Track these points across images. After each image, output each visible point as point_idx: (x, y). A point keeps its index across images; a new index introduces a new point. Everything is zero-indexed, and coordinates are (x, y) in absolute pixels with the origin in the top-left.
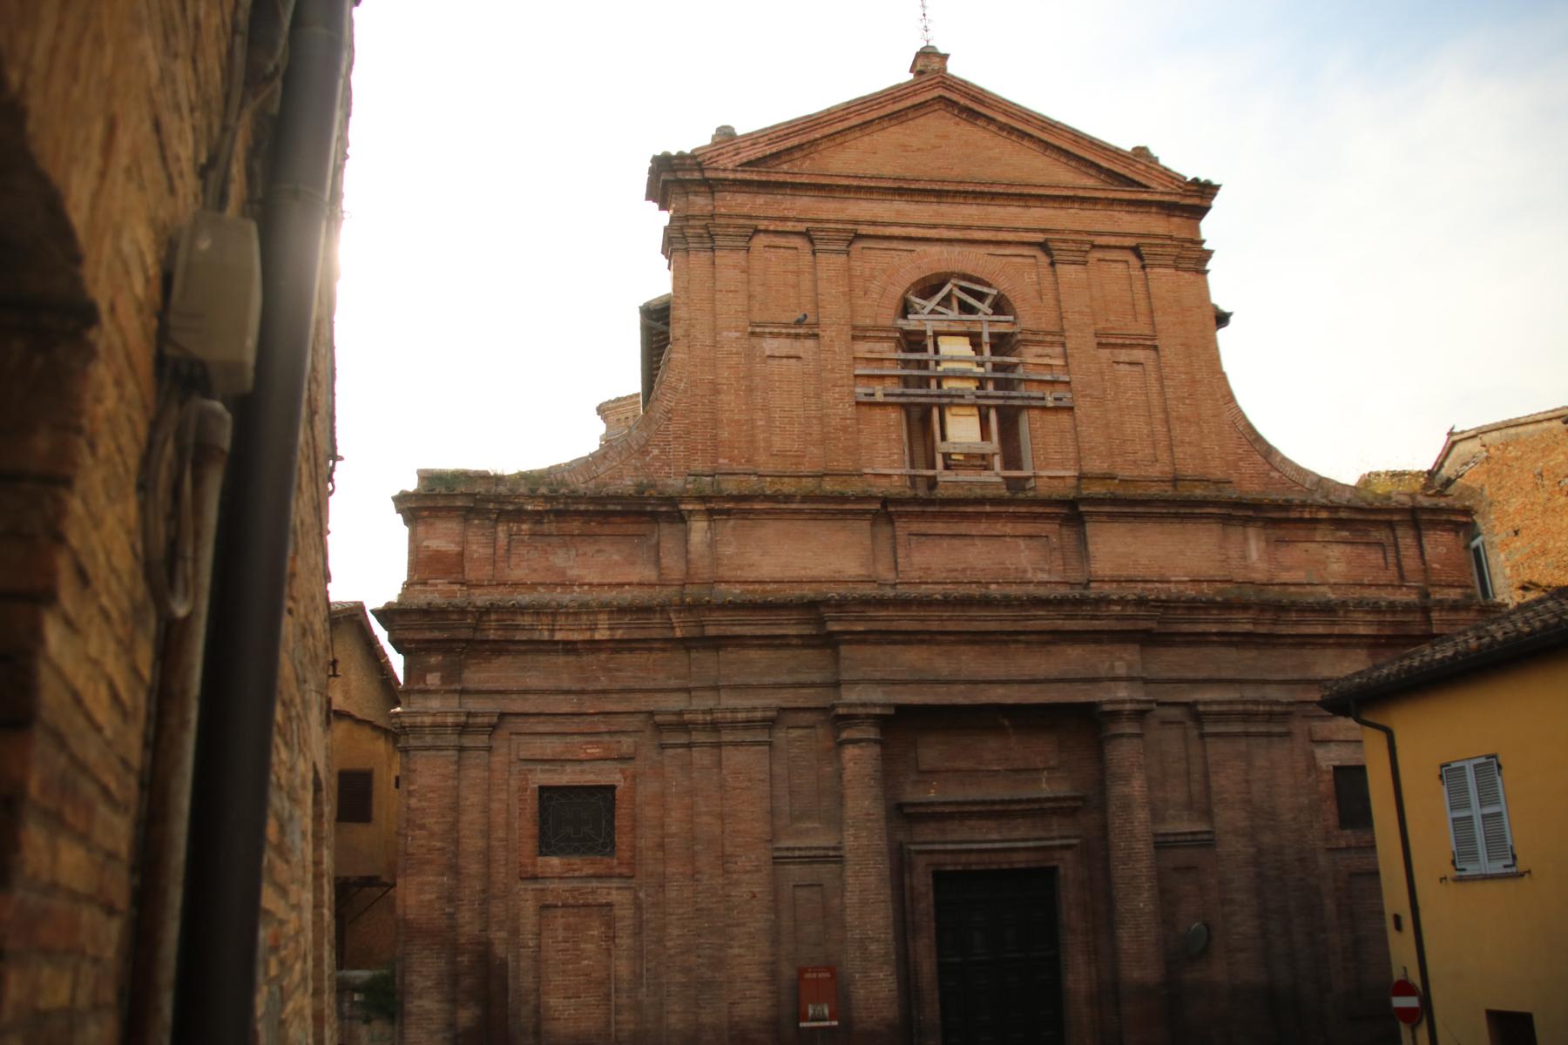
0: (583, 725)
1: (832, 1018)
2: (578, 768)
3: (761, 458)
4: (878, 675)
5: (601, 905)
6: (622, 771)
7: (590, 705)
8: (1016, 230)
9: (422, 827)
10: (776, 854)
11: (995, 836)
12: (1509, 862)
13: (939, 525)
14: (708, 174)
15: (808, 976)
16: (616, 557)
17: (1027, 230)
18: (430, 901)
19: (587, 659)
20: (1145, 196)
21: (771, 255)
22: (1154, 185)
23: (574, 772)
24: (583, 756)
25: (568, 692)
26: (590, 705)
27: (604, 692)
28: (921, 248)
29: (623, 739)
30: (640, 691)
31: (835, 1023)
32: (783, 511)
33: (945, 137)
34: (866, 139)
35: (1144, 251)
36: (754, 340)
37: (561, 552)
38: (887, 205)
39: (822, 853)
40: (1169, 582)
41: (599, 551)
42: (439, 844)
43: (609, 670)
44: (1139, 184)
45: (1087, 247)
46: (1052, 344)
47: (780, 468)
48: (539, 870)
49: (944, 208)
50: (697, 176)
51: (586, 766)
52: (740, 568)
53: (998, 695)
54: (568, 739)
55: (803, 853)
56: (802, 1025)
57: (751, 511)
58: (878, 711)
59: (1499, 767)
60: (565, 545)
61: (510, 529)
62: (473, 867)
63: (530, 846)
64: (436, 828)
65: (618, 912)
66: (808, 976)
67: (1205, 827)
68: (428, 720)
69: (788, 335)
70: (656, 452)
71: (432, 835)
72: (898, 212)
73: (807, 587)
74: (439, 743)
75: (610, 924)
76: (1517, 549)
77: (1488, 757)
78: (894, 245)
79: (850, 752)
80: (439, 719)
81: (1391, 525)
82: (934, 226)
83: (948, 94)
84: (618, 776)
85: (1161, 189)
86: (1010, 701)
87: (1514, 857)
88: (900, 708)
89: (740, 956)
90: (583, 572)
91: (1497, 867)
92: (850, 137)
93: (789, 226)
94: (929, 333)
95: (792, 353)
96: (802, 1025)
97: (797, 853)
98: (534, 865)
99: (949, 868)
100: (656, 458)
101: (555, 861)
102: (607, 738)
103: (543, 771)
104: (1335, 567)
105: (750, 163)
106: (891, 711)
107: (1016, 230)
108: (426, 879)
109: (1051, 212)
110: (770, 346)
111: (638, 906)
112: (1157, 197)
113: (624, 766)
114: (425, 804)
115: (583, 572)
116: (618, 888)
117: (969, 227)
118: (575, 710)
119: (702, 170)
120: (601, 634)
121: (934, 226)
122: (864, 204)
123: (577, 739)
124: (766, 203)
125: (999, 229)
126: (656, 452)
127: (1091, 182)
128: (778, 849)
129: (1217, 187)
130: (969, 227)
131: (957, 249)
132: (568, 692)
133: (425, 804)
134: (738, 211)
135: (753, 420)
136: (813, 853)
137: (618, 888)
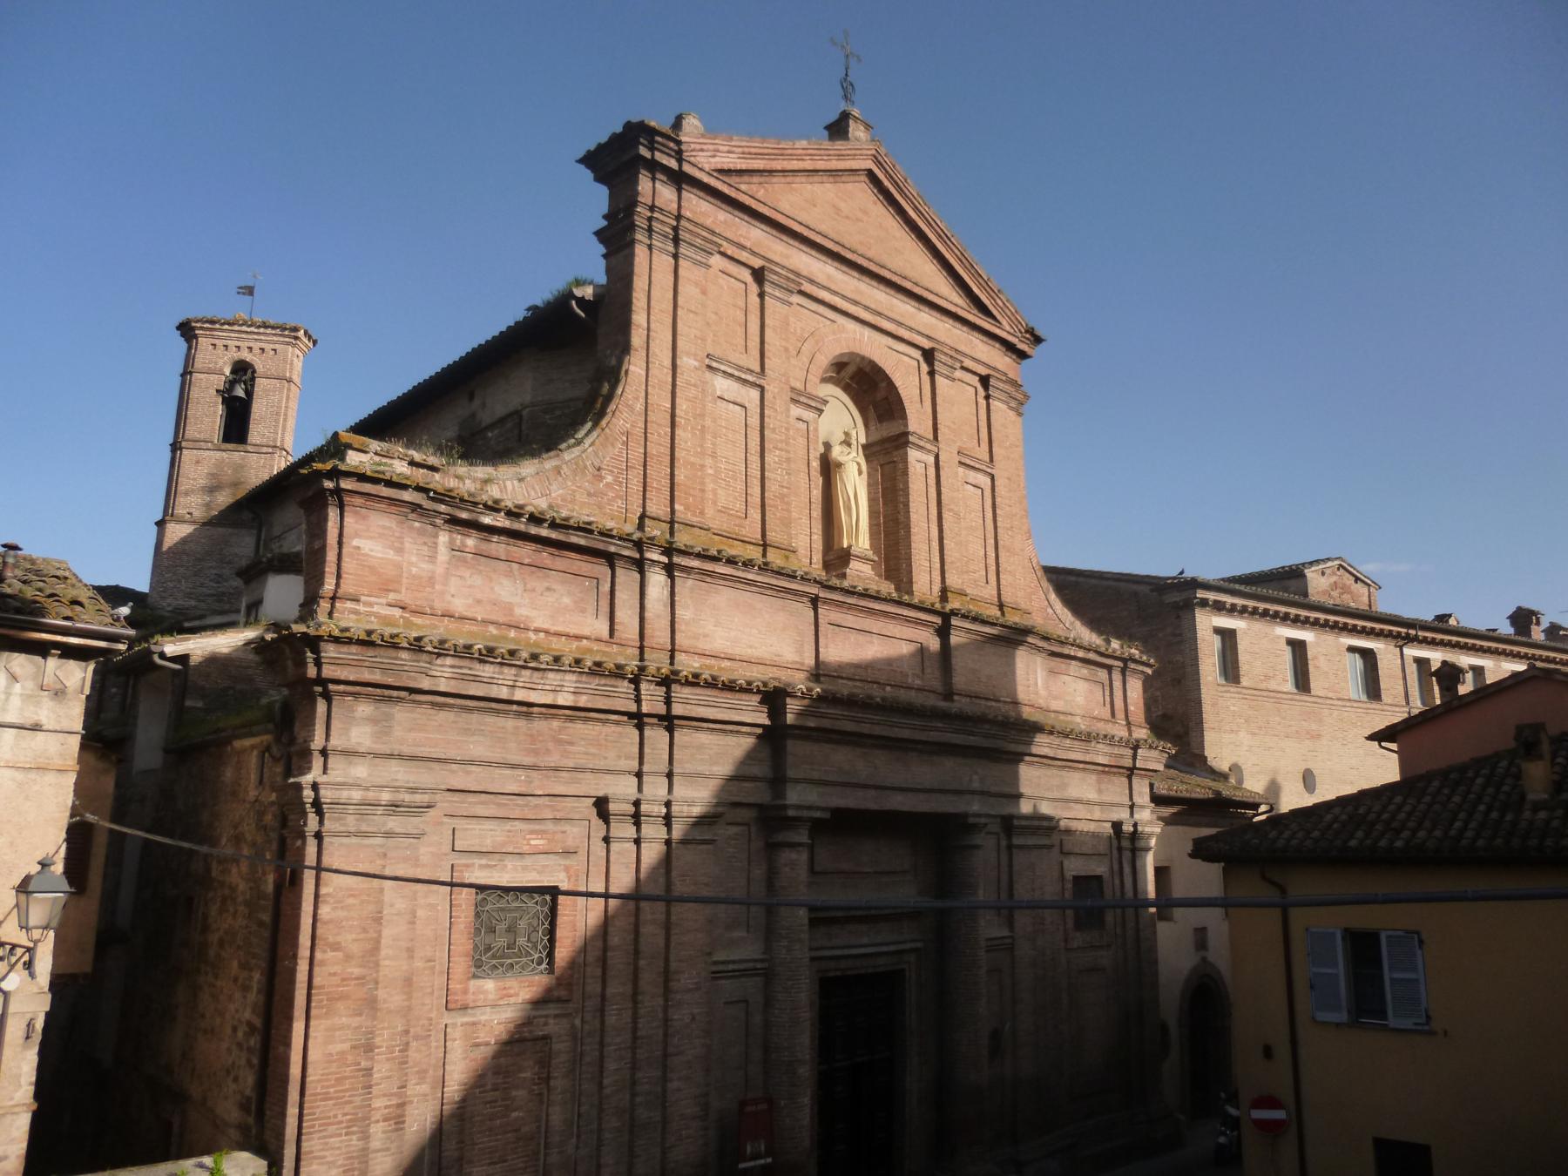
0: (517, 808)
1: (767, 1155)
2: (518, 863)
3: (710, 512)
4: (815, 775)
5: (536, 1039)
6: (567, 869)
7: (539, 784)
9: (336, 947)
10: (714, 968)
11: (865, 941)
12: (1423, 1020)
14: (687, 168)
15: (749, 1109)
16: (566, 600)
18: (343, 1053)
19: (540, 725)
21: (723, 280)
22: (1004, 323)
23: (515, 869)
24: (526, 849)
25: (514, 766)
26: (539, 784)
27: (556, 769)
29: (567, 827)
30: (593, 771)
31: (769, 1160)
32: (740, 580)
33: (865, 212)
34: (809, 187)
35: (992, 382)
36: (708, 375)
39: (751, 965)
40: (998, 701)
41: (548, 589)
42: (357, 971)
43: (560, 742)
44: (994, 318)
45: (958, 365)
48: (470, 997)
50: (673, 164)
51: (528, 861)
53: (898, 802)
54: (508, 826)
55: (735, 967)
56: (742, 1166)
58: (818, 814)
59: (1421, 942)
61: (452, 541)
62: (391, 998)
63: (461, 965)
64: (355, 949)
65: (556, 1047)
66: (749, 1109)
67: (1006, 933)
68: (356, 795)
70: (609, 479)
71: (348, 957)
73: (755, 668)
74: (364, 828)
75: (545, 1063)
76: (474, 480)
77: (1407, 932)
78: (821, 309)
79: (787, 856)
80: (371, 795)
82: (856, 303)
84: (562, 875)
86: (905, 809)
87: (1428, 1017)
88: (838, 813)
89: (679, 1090)
90: (533, 614)
91: (1408, 1023)
93: (744, 256)
96: (742, 1166)
97: (731, 967)
98: (465, 992)
99: (831, 974)
100: (608, 485)
101: (489, 985)
102: (550, 826)
103: (482, 867)
106: (827, 815)
108: (337, 1021)
109: (933, 320)
110: (722, 385)
111: (574, 1036)
113: (567, 862)
114: (341, 914)
115: (533, 614)
116: (556, 1016)
117: (880, 314)
118: (523, 790)
119: (680, 161)
120: (564, 699)
121: (856, 303)
122: (805, 258)
123: (519, 825)
125: (900, 324)
126: (609, 479)
127: (960, 301)
128: (716, 963)
129: (589, 160)
130: (880, 314)
131: (867, 332)
132: (514, 766)
133: (341, 914)
135: (703, 466)
136: (742, 966)
137: (556, 1016)
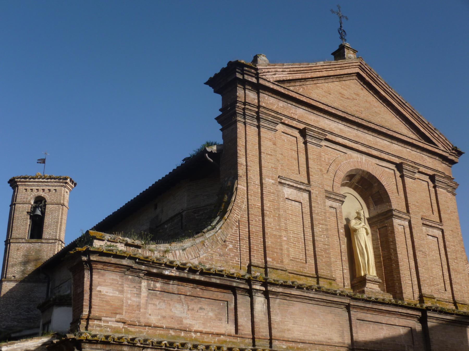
3: (286, 261)
8: (388, 154)
13: (369, 315)
14: (261, 82)
16: (211, 314)
17: (393, 155)
20: (436, 150)
21: (284, 137)
22: (440, 145)
28: (349, 152)
33: (358, 95)
34: (326, 84)
36: (280, 187)
37: (178, 306)
38: (336, 124)
41: (201, 308)
45: (416, 171)
46: (405, 219)
47: (295, 268)
49: (360, 133)
52: (283, 331)
57: (290, 295)
60: (180, 301)
61: (149, 285)
69: (296, 188)
70: (231, 246)
72: (341, 130)
78: (338, 147)
81: (234, 290)
82: (357, 142)
83: (361, 73)
85: (442, 148)
90: (193, 322)
92: (320, 81)
93: (294, 123)
94: (344, 200)
95: (297, 199)
104: (243, 310)
105: (279, 81)
107: (388, 154)
110: (288, 192)
112: (440, 152)
115: (193, 322)
119: (258, 78)
121: (357, 142)
124: (283, 107)
126: (231, 246)
127: (414, 137)
134: (270, 107)
